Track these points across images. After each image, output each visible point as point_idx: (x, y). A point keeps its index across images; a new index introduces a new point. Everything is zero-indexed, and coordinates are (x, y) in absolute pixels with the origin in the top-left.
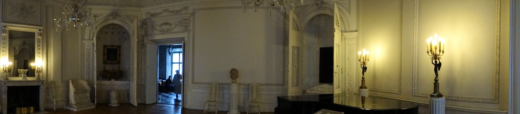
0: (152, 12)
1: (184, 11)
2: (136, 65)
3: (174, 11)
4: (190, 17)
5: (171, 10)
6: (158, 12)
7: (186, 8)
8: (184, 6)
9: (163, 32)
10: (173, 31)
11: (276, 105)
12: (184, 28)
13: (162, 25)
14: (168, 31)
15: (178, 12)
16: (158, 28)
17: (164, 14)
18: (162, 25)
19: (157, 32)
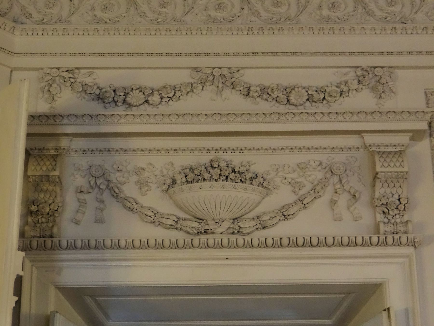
0: (105, 79)
1: (364, 99)
2: (416, 277)
3: (288, 91)
4: (416, 135)
5: (252, 78)
6: (151, 79)
7: (375, 79)
8: (365, 61)
9: (199, 231)
10: (283, 230)
11: (14, 305)
12: (366, 216)
13: (194, 176)
14: (240, 233)
15: (317, 96)
16: (153, 199)
17: (203, 100)
18: (194, 176)
19: (142, 231)
